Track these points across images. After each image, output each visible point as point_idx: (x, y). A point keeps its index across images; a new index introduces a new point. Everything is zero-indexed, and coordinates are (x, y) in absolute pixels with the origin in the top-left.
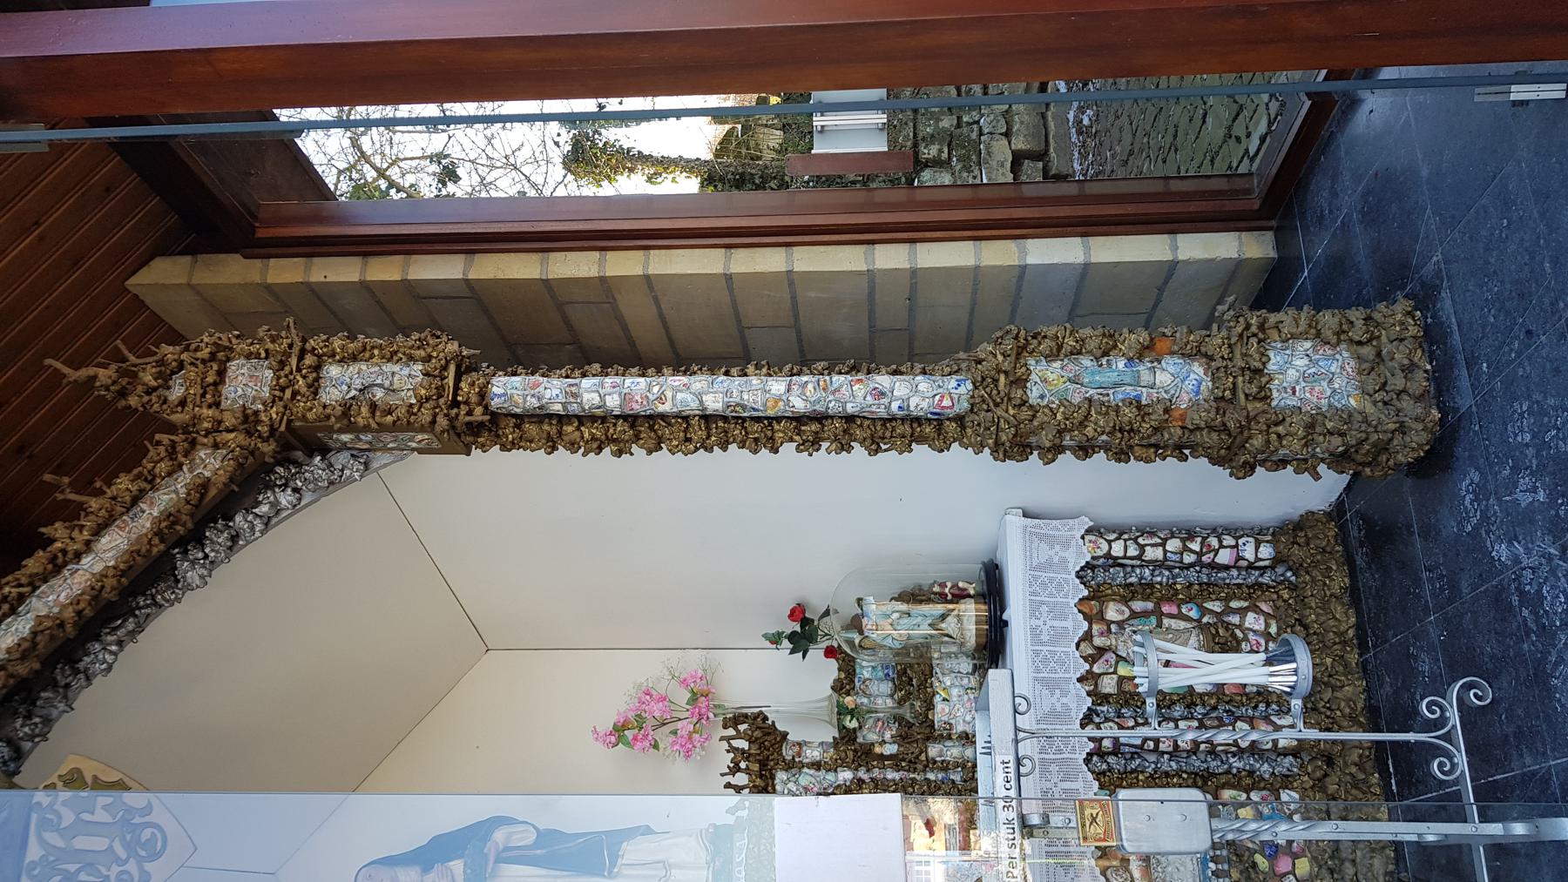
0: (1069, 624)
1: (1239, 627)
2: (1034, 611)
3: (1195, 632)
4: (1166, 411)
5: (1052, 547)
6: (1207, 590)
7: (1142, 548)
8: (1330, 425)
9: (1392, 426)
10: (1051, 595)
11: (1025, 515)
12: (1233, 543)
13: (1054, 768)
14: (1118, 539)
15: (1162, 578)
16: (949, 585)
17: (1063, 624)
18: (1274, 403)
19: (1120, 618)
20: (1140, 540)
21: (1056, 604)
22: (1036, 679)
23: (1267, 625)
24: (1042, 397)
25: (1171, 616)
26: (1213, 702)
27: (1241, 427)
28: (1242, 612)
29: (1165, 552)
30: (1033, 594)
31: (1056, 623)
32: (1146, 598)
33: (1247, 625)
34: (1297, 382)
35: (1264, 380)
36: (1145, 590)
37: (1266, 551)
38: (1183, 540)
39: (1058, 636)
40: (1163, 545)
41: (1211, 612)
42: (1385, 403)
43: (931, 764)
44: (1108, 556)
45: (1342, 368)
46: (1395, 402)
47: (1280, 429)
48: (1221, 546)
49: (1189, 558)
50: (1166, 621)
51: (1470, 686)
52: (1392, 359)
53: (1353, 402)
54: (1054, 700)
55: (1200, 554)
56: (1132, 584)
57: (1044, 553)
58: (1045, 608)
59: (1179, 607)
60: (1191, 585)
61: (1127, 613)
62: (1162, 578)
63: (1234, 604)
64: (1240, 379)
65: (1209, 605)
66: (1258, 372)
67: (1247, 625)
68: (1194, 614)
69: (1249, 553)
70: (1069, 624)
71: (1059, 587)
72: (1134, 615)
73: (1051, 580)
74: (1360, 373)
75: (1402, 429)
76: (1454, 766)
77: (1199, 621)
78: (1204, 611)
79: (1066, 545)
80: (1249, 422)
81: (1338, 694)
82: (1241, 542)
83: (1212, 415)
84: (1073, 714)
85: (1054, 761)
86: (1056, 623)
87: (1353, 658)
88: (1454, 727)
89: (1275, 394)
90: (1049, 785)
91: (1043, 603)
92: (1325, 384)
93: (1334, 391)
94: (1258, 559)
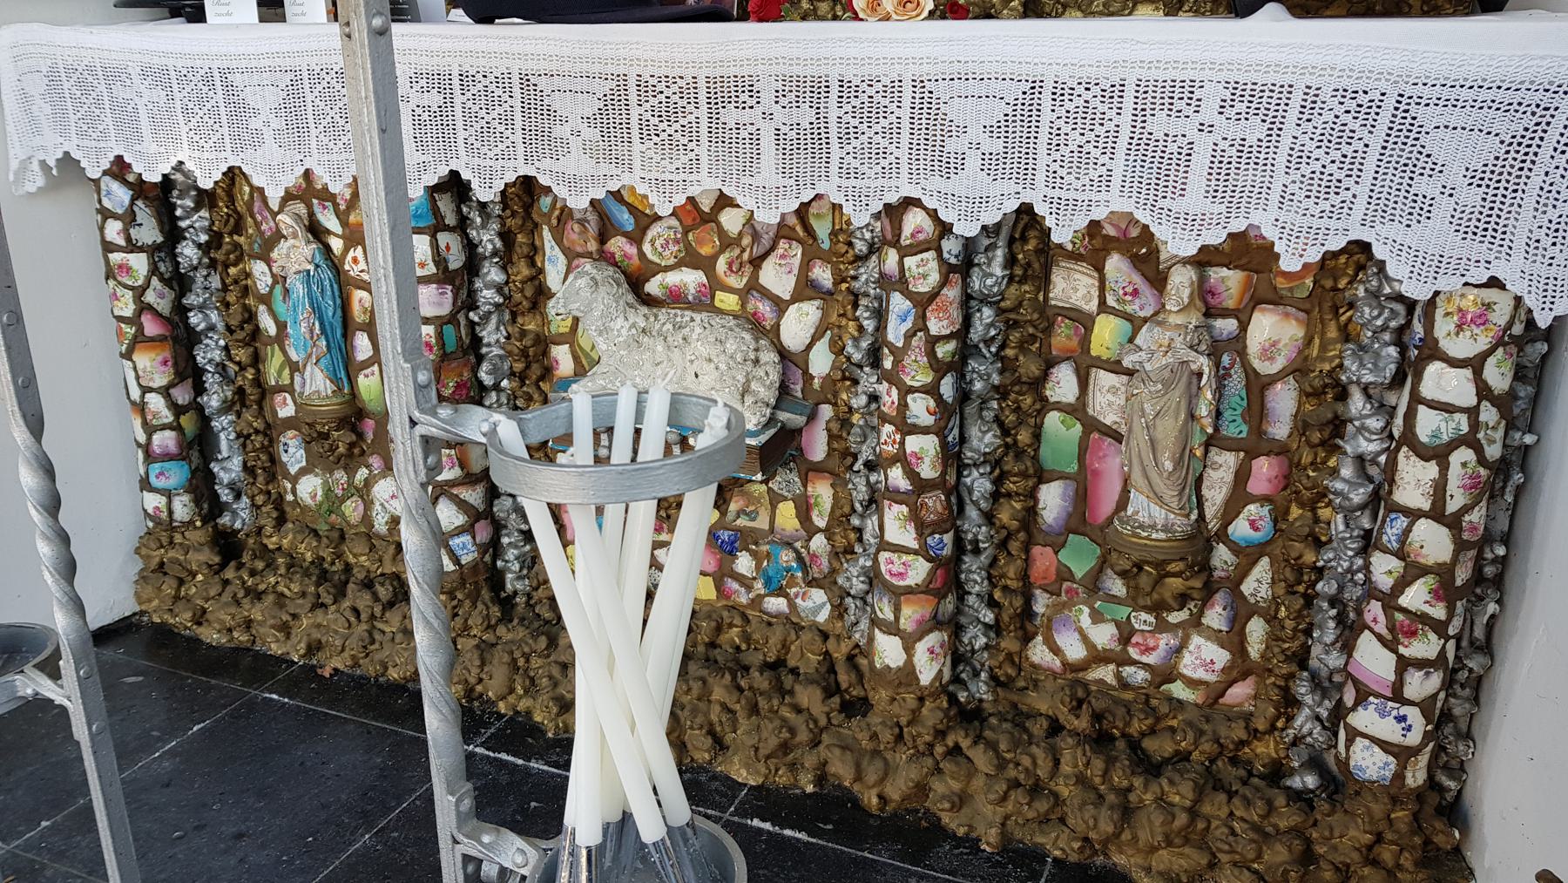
0: (1195, 199)
1: (1196, 622)
2: (1245, 97)
3: (1181, 524)
5: (1476, 178)
6: (1299, 582)
7: (1439, 454)
10: (1298, 157)
14: (1484, 391)
15: (1347, 484)
22: (1036, 87)
23: (1192, 683)
25: (1242, 475)
26: (1004, 516)
28: (1234, 639)
29: (1414, 515)
31: (1201, 161)
32: (1301, 425)
33: (1196, 640)
37: (1369, 763)
38: (1444, 573)
39: (1162, 166)
40: (1437, 513)
41: (1243, 573)
48: (1404, 664)
54: (976, 133)
55: (1389, 601)
59: (1264, 499)
61: (1265, 368)
62: (1347, 484)
63: (1256, 629)
67: (1196, 640)
68: (1240, 529)
70: (1195, 199)
72: (1258, 386)
73: (1354, 166)
77: (1222, 536)
78: (1248, 555)
79: (1486, 226)
82: (1414, 714)
84: (547, 163)
86: (1201, 161)
90: (767, 97)
91: (1275, 129)
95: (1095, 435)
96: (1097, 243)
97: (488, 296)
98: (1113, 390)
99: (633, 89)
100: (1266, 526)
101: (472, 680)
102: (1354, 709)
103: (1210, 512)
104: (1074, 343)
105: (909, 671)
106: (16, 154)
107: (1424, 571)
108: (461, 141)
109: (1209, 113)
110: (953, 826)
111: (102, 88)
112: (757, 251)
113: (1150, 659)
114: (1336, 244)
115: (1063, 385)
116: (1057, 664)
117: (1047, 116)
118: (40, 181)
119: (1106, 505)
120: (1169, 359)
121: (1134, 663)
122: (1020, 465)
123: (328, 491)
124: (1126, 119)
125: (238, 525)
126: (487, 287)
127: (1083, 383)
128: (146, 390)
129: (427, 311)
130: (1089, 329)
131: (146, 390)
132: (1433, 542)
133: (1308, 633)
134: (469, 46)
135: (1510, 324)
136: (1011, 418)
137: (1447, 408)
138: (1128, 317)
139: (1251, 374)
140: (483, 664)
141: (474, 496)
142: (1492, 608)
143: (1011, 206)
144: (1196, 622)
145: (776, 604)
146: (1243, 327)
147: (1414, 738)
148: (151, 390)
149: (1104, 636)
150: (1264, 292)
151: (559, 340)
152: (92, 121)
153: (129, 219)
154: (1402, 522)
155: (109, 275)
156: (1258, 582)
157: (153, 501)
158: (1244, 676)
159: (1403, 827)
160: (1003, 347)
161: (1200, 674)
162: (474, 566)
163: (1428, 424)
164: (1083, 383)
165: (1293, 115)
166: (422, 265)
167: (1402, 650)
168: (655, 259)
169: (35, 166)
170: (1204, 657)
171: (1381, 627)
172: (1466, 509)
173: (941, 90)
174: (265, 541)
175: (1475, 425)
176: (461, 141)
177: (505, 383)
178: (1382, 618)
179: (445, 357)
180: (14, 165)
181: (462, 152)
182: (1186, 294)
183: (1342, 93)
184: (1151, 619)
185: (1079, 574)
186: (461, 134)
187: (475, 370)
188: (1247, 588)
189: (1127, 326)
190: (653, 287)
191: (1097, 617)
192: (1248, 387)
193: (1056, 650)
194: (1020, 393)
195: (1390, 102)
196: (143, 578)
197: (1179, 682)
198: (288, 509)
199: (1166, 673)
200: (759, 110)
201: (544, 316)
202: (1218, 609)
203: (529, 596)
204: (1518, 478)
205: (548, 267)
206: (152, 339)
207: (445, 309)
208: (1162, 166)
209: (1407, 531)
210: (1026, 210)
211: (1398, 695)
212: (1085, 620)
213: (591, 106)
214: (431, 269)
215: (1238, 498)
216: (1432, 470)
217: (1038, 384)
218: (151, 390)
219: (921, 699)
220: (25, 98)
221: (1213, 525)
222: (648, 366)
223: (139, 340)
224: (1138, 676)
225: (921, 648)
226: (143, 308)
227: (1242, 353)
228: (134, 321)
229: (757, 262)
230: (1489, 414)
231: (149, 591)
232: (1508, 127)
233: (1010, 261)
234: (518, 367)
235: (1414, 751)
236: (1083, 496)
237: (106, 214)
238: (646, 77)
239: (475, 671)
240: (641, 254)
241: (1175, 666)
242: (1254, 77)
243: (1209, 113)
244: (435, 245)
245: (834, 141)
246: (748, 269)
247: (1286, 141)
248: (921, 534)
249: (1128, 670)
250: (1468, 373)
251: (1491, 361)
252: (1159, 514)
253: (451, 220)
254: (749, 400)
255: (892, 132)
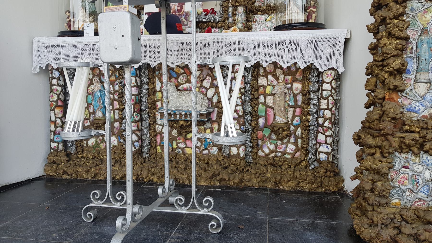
0: (286, 59)
1: (289, 142)
2: (292, 42)
3: (286, 121)
4: (396, 87)
5: (328, 52)
6: (306, 129)
7: (327, 98)
8: (379, 184)
9: (375, 219)
10: (301, 51)
11: (347, 41)
12: (328, 142)
13: (219, 48)
14: (332, 87)
16: (315, 10)
17: (286, 56)
18: (397, 154)
19: (294, 88)
20: (330, 98)
21: (297, 53)
22: (259, 42)
23: (289, 154)
24: (412, 10)
25: (294, 112)
26: (253, 124)
27: (380, 130)
28: (296, 144)
29: (324, 109)
30: (302, 42)
31: (286, 52)
32: (303, 102)
33: (289, 145)
34: (412, 170)
35: (416, 150)
36: (307, 102)
37: (323, 157)
38: (330, 119)
39: (281, 54)
40: (328, 109)
42: (392, 219)
43: (235, 7)
44: (323, 82)
45: (421, 199)
46: (392, 225)
47: (378, 155)
48: (326, 136)
49: (321, 121)
50: (291, 110)
51: (219, 226)
52: (426, 231)
53: (395, 201)
55: (322, 126)
56: (310, 95)
57: (325, 48)
58: (294, 47)
59: (299, 116)
60: (309, 122)
63: (299, 141)
64: (417, 135)
65: (299, 129)
66: (421, 147)
67: (289, 145)
68: (295, 122)
69: (322, 148)
70: (286, 59)
71: (305, 55)
72: (295, 96)
73: (310, 51)
74: (416, 209)
75: (372, 224)
76: (181, 206)
77: (292, 124)
78: (297, 127)
79: (329, 59)
80: (383, 135)
81: (253, 176)
82: (329, 146)
83: (391, 115)
85: (222, 48)
86: (286, 52)
87: (269, 185)
88: (199, 211)
89: (404, 156)
90: (212, 45)
91: (297, 47)
92: (410, 186)
93: (404, 192)
94: (320, 152)
95: (268, 108)
96: (266, 73)
97: (144, 92)
98: (271, 99)
99: (185, 45)
100: (299, 121)
101: (139, 174)
102: (319, 147)
103: (289, 120)
104: (263, 91)
105: (238, 154)
106: (35, 64)
107: (327, 119)
108: (148, 56)
109: (287, 45)
110: (249, 185)
111: (61, 49)
112: (203, 78)
113: (281, 150)
114: (308, 64)
115: (262, 99)
116: (264, 155)
117: (261, 46)
118: (38, 70)
119: (271, 121)
120: (281, 91)
121: (278, 152)
122: (255, 116)
123: (96, 142)
124: (274, 46)
125: (72, 152)
126: (144, 89)
127: (265, 98)
128: (56, 118)
129: (133, 93)
130: (265, 89)
131: (56, 118)
132: (328, 114)
133: (309, 139)
134: (152, 38)
135: (334, 76)
136: (253, 105)
137: (327, 90)
138: (272, 86)
139: (294, 93)
140: (141, 171)
141: (139, 133)
142: (338, 129)
143: (256, 62)
144: (289, 142)
145: (206, 152)
146: (292, 86)
147: (330, 151)
148: (57, 118)
149: (272, 147)
150: (295, 79)
151: (158, 100)
152: (56, 56)
153: (58, 79)
154: (323, 111)
155: (52, 91)
156: (299, 132)
157: (53, 145)
158: (298, 151)
159: (330, 167)
160: (251, 92)
161: (291, 152)
162: (139, 149)
163: (325, 94)
164: (265, 98)
165: (300, 44)
166: (133, 83)
167: (326, 134)
168: (181, 82)
169: (38, 67)
170: (291, 148)
171: (322, 131)
172: (332, 107)
173: (243, 43)
174: (78, 156)
175: (332, 93)
176: (148, 56)
177: (147, 110)
178: (322, 129)
179: (136, 103)
180: (34, 66)
181: (148, 58)
182: (283, 79)
183: (307, 41)
184: (280, 142)
185: (267, 136)
186: (148, 55)
187: (141, 106)
188: (297, 134)
189: (272, 87)
190: (180, 87)
191: (271, 144)
192: (294, 96)
193: (263, 152)
194: (255, 100)
195: (314, 42)
196: (46, 165)
197: (287, 155)
198: (84, 148)
199: (284, 153)
200: (210, 48)
201: (155, 96)
202: (292, 138)
203: (149, 158)
204: (339, 105)
205: (157, 86)
206: (60, 106)
207: (137, 93)
208: (281, 54)
209: (324, 112)
210: (258, 62)
211: (326, 143)
212: (269, 144)
213: (176, 48)
214: (135, 84)
215: (294, 117)
216: (326, 101)
217: (258, 98)
218: (57, 118)
219: (241, 160)
220: (39, 52)
221: (290, 122)
222: (181, 101)
223: (57, 106)
224: (279, 154)
225: (241, 149)
226: (59, 99)
227: (292, 90)
228: (57, 102)
229: (202, 81)
230: (333, 91)
231: (49, 168)
232: (331, 44)
233: (252, 76)
234: (150, 106)
235: (330, 153)
236: (267, 120)
237: (53, 78)
238: (188, 42)
239: (140, 172)
240: (178, 81)
241: (286, 151)
242: (293, 39)
243: (287, 45)
244: (136, 79)
245: (224, 52)
246: (201, 82)
247: (299, 48)
248: (240, 126)
249: (277, 153)
250: (329, 84)
251: (333, 82)
252: (281, 119)
253: (139, 75)
254: (203, 106)
255: (234, 50)
